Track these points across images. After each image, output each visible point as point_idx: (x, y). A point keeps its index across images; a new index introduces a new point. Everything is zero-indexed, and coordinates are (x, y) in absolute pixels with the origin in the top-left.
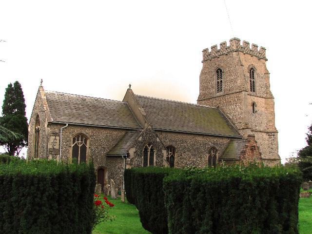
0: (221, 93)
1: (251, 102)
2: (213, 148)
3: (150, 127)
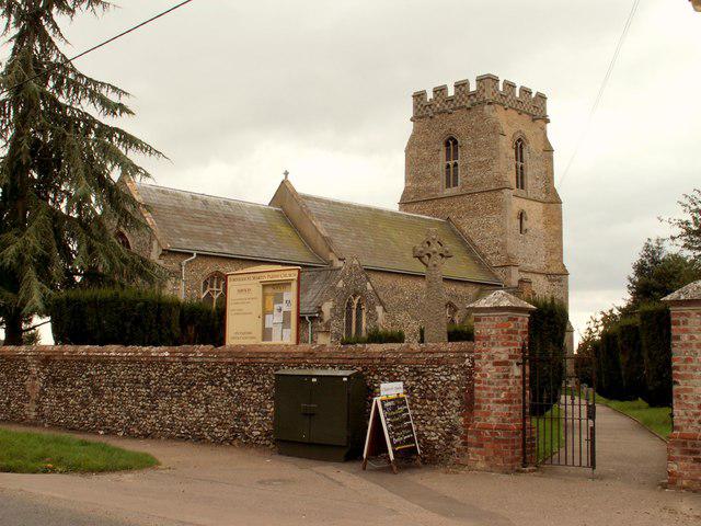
2: (450, 305)
3: (355, 262)
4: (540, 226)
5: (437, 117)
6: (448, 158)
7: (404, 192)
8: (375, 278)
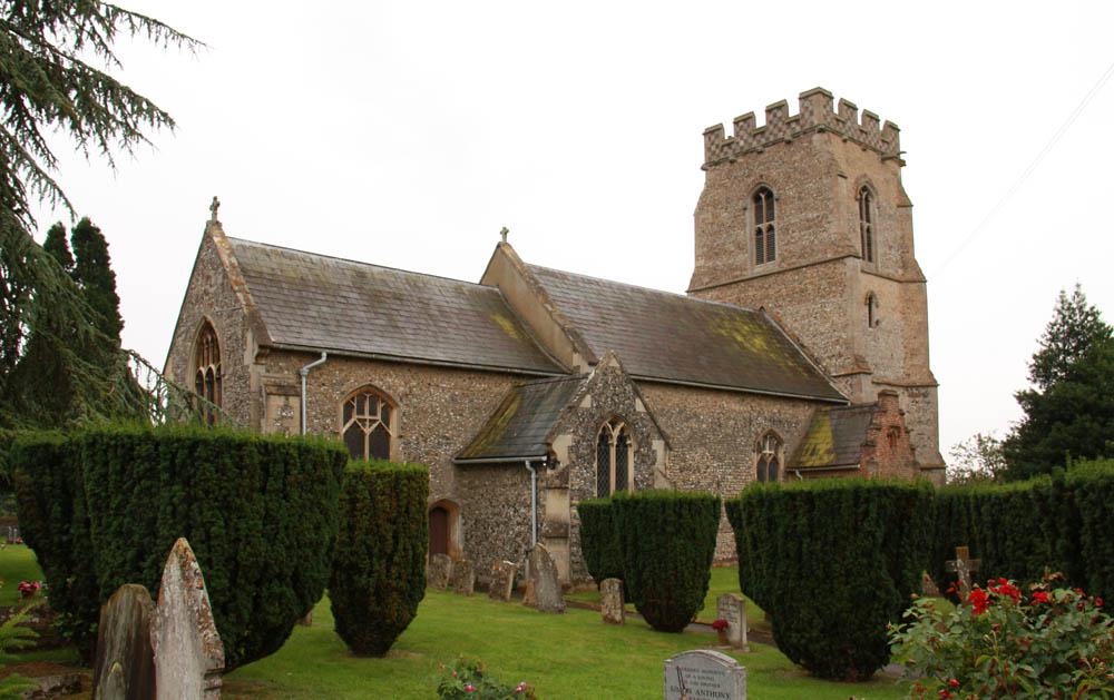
0: (770, 267)
1: (864, 292)
3: (614, 363)
4: (897, 316)
5: (740, 160)
6: (759, 220)
7: (694, 275)
8: (652, 395)
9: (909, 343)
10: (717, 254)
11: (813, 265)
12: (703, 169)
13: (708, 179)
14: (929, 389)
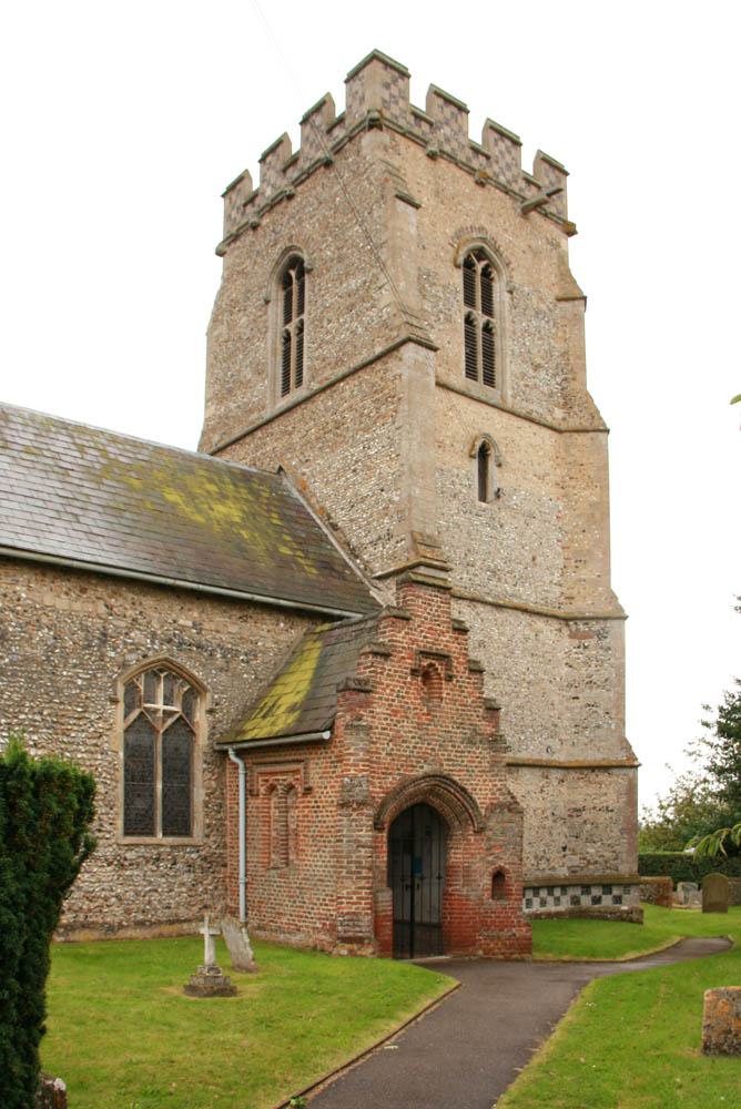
4: (546, 490)
9: (572, 540)
10: (230, 391)
11: (355, 371)
12: (220, 253)
13: (226, 268)
14: (609, 624)
